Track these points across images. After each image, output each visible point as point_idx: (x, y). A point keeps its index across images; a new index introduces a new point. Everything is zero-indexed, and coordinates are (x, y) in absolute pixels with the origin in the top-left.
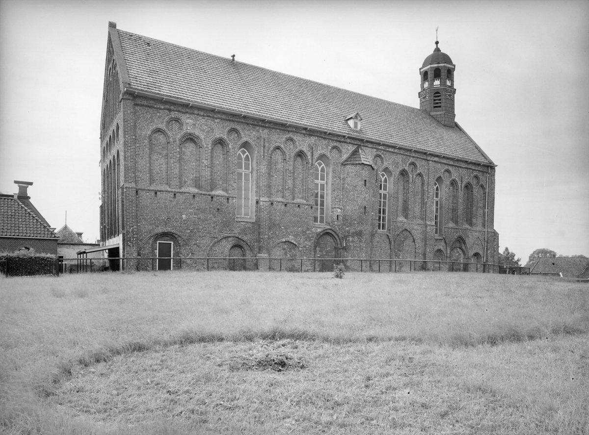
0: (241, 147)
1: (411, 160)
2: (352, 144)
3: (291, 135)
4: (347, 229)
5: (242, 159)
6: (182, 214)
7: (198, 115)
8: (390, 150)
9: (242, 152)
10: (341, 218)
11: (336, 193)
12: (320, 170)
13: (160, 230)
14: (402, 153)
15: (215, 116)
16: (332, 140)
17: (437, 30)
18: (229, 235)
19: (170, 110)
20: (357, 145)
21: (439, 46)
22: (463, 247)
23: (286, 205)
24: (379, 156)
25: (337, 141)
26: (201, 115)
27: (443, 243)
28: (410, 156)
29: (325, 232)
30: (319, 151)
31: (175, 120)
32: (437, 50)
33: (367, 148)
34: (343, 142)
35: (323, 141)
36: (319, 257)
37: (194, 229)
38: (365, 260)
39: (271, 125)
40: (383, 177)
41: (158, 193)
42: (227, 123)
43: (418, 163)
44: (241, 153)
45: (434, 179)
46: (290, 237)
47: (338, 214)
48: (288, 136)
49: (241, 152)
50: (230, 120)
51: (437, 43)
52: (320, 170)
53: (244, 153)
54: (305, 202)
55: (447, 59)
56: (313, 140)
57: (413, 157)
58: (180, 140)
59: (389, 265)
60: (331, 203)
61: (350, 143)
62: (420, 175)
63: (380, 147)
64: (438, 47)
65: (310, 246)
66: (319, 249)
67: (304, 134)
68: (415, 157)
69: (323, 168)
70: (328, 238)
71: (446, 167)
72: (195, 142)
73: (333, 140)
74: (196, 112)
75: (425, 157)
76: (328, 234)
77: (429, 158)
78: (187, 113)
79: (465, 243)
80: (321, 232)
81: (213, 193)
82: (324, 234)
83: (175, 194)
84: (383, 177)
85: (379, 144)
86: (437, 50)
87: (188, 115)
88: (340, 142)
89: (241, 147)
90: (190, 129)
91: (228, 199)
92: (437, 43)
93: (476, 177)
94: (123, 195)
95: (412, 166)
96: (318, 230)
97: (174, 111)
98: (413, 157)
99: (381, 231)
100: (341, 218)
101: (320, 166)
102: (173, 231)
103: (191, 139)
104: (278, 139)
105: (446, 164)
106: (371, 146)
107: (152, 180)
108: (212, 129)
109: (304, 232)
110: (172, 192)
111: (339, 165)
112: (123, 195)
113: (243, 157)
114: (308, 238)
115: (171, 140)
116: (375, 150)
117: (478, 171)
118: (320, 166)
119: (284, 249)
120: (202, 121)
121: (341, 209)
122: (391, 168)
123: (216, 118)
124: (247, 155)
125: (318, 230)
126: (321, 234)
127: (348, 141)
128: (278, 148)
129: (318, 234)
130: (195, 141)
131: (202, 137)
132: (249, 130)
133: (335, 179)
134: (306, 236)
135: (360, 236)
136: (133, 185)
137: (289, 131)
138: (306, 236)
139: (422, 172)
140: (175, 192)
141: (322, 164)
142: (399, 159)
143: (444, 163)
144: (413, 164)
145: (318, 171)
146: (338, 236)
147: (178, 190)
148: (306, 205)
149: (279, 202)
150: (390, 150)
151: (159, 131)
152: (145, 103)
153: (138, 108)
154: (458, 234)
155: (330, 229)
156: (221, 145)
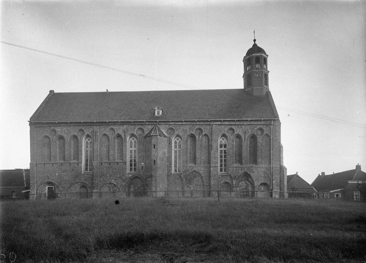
0: (221, 137)
1: (197, 127)
2: (150, 125)
3: (112, 127)
5: (132, 143)
8: (179, 123)
9: (177, 139)
10: (144, 168)
12: (133, 142)
17: (254, 32)
18: (79, 181)
19: (50, 127)
20: (154, 125)
21: (256, 42)
22: (250, 180)
24: (172, 128)
25: (140, 125)
27: (229, 178)
28: (196, 125)
29: (135, 176)
32: (255, 45)
34: (144, 125)
36: (133, 190)
37: (61, 180)
38: (154, 191)
39: (100, 124)
40: (178, 141)
41: (46, 165)
42: (77, 127)
43: (264, 128)
44: (176, 140)
46: (113, 180)
50: (78, 126)
51: (255, 40)
52: (133, 142)
53: (133, 139)
54: (121, 161)
55: (261, 50)
56: (125, 127)
57: (199, 125)
59: (182, 193)
61: (149, 125)
62: (206, 135)
64: (256, 43)
65: (125, 185)
66: (133, 186)
68: (200, 125)
69: (135, 141)
70: (138, 179)
71: (229, 127)
72: (62, 139)
73: (138, 125)
74: (61, 125)
75: (208, 123)
76: (137, 177)
77: (212, 123)
78: (57, 126)
79: (251, 177)
80: (131, 177)
81: (70, 162)
82: (134, 178)
84: (178, 141)
86: (255, 45)
87: (58, 127)
88: (142, 125)
89: (221, 137)
90: (59, 133)
91: (78, 164)
92: (255, 40)
93: (261, 129)
95: (199, 131)
96: (130, 176)
97: (51, 126)
98: (199, 125)
99: (223, 173)
100: (144, 168)
102: (52, 181)
104: (107, 130)
105: (228, 125)
108: (69, 131)
109: (120, 178)
110: (51, 163)
114: (124, 181)
116: (168, 125)
117: (262, 125)
119: (109, 187)
120: (65, 128)
121: (144, 163)
122: (180, 134)
123: (72, 126)
124: (180, 140)
126: (132, 178)
127: (148, 123)
129: (130, 178)
132: (89, 128)
134: (122, 179)
135: (152, 177)
136: (77, 162)
137: (110, 125)
138: (122, 179)
139: (207, 133)
142: (187, 128)
143: (226, 125)
144: (261, 129)
148: (121, 162)
149: (105, 163)
154: (243, 171)
155: (138, 175)
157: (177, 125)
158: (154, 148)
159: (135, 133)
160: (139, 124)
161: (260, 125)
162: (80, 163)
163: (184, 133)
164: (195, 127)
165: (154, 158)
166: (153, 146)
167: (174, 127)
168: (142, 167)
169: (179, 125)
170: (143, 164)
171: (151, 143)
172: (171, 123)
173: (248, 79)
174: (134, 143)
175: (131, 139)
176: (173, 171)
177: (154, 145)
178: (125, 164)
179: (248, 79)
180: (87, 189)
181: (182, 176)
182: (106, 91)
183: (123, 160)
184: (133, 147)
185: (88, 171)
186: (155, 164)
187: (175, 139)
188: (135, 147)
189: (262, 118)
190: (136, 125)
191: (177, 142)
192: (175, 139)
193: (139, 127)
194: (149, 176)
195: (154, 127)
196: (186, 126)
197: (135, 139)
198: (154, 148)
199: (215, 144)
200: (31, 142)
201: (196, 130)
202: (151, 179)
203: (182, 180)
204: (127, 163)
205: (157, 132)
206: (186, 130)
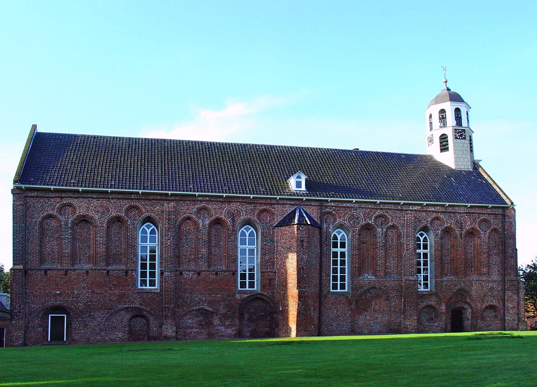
6: (73, 289)
7: (92, 198)
8: (344, 205)
13: (51, 302)
15: (110, 197)
16: (259, 203)
19: (62, 198)
23: (199, 274)
25: (265, 204)
26: (94, 198)
30: (242, 217)
31: (67, 206)
41: (48, 272)
52: (422, 241)
53: (149, 227)
58: (72, 222)
67: (222, 202)
83: (66, 272)
84: (247, 232)
94: (271, 361)
101: (422, 237)
103: (84, 220)
105: (433, 212)
107: (42, 260)
110: (63, 270)
112: (271, 361)
115: (63, 223)
117: (489, 214)
118: (422, 237)
120: (95, 202)
128: (189, 218)
130: (221, 223)
131: (97, 217)
137: (201, 201)
140: (66, 269)
147: (70, 268)
150: (344, 205)
151: (50, 217)
152: (35, 194)
153: (29, 200)
156: (220, 225)
161: (485, 214)
162: (132, 270)
163: (354, 222)
164: (375, 213)
169: (344, 207)
172: (330, 204)
173: (442, 140)
179: (442, 140)
180: (148, 321)
182: (469, 167)
185: (247, 288)
189: (402, 200)
191: (337, 237)
199: (411, 242)
201: (376, 218)
206: (358, 218)
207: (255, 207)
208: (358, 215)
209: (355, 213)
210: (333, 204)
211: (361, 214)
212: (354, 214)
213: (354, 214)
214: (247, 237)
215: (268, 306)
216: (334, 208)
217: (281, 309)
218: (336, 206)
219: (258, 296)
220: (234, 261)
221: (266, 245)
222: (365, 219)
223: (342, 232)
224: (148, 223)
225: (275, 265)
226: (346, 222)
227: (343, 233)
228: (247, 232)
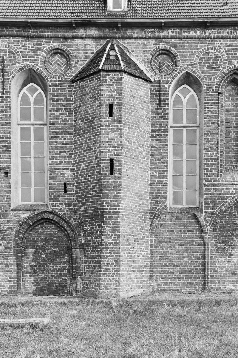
4: (83, 208)
8: (192, 33)
9: (181, 92)
11: (59, 141)
14: (150, 34)
24: (167, 53)
25: (56, 38)
30: (18, 65)
33: (130, 41)
35: (26, 42)
45: (100, 78)
47: (65, 180)
48: (55, 44)
49: (180, 92)
60: (50, 162)
63: (165, 33)
66: (33, 250)
76: (48, 220)
80: (29, 218)
85: (160, 26)
96: (22, 216)
100: (71, 188)
106: (143, 34)
111: (66, 85)
113: (32, 99)
116: (154, 41)
122: (197, 72)
125: (22, 216)
133: (57, 114)
141: (38, 90)
145: (29, 104)
146: (69, 225)
157: (186, 38)
158: (111, 114)
159: (39, 67)
160: (62, 34)
165: (108, 153)
166: (105, 110)
167: (175, 46)
168: (65, 184)
170: (68, 174)
171: (97, 97)
174: (35, 103)
175: (24, 90)
176: (169, 202)
177: (111, 106)
178: (6, 173)
181: (202, 217)
183: (218, 90)
184: (32, 119)
186: (112, 173)
187: (176, 88)
188: (38, 117)
190: (42, 37)
192: (176, 88)
193: (55, 44)
194: (91, 216)
195: (107, 44)
196: (217, 44)
197: (40, 90)
198: (111, 114)
200: (181, 23)
202: (99, 226)
203: (202, 231)
204: (12, 173)
205: (120, 64)
207: (38, 45)
208: (217, 53)
209: (212, 49)
210: (171, 34)
211: (222, 50)
212: (210, 51)
213: (210, 51)
214: (32, 106)
215: (65, 234)
216: (173, 40)
217: (83, 242)
218: (176, 38)
219: (50, 216)
220: (6, 150)
221: (57, 118)
222: (230, 61)
223: (38, 90)
224: (31, 84)
225: (73, 156)
226: (194, 69)
227: (193, 92)
228: (185, 98)
